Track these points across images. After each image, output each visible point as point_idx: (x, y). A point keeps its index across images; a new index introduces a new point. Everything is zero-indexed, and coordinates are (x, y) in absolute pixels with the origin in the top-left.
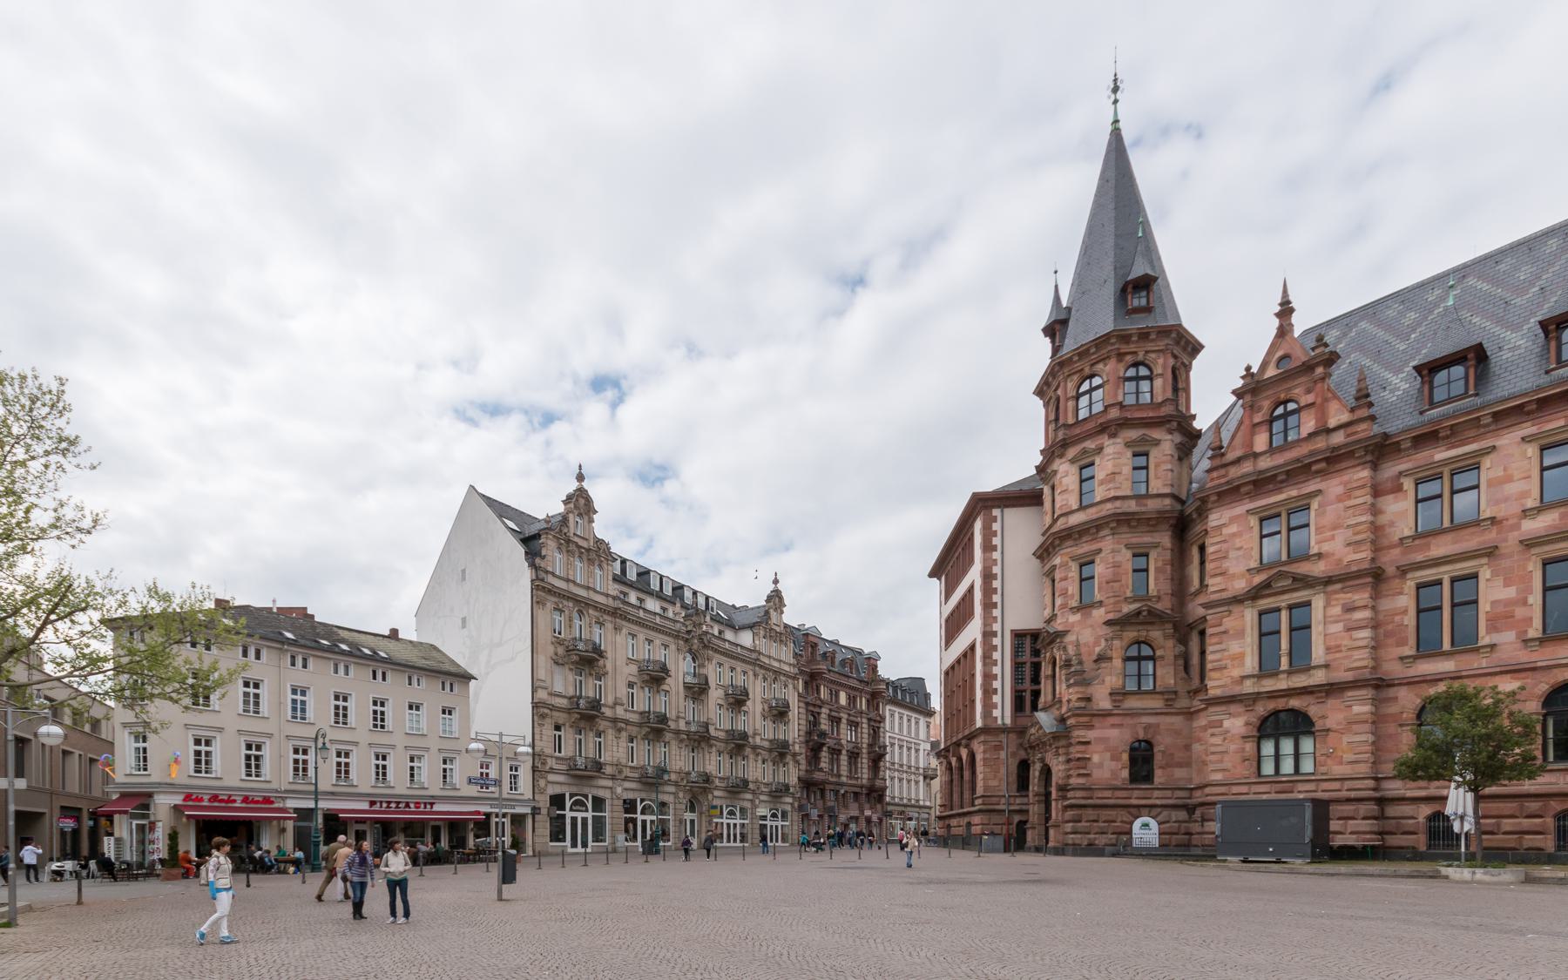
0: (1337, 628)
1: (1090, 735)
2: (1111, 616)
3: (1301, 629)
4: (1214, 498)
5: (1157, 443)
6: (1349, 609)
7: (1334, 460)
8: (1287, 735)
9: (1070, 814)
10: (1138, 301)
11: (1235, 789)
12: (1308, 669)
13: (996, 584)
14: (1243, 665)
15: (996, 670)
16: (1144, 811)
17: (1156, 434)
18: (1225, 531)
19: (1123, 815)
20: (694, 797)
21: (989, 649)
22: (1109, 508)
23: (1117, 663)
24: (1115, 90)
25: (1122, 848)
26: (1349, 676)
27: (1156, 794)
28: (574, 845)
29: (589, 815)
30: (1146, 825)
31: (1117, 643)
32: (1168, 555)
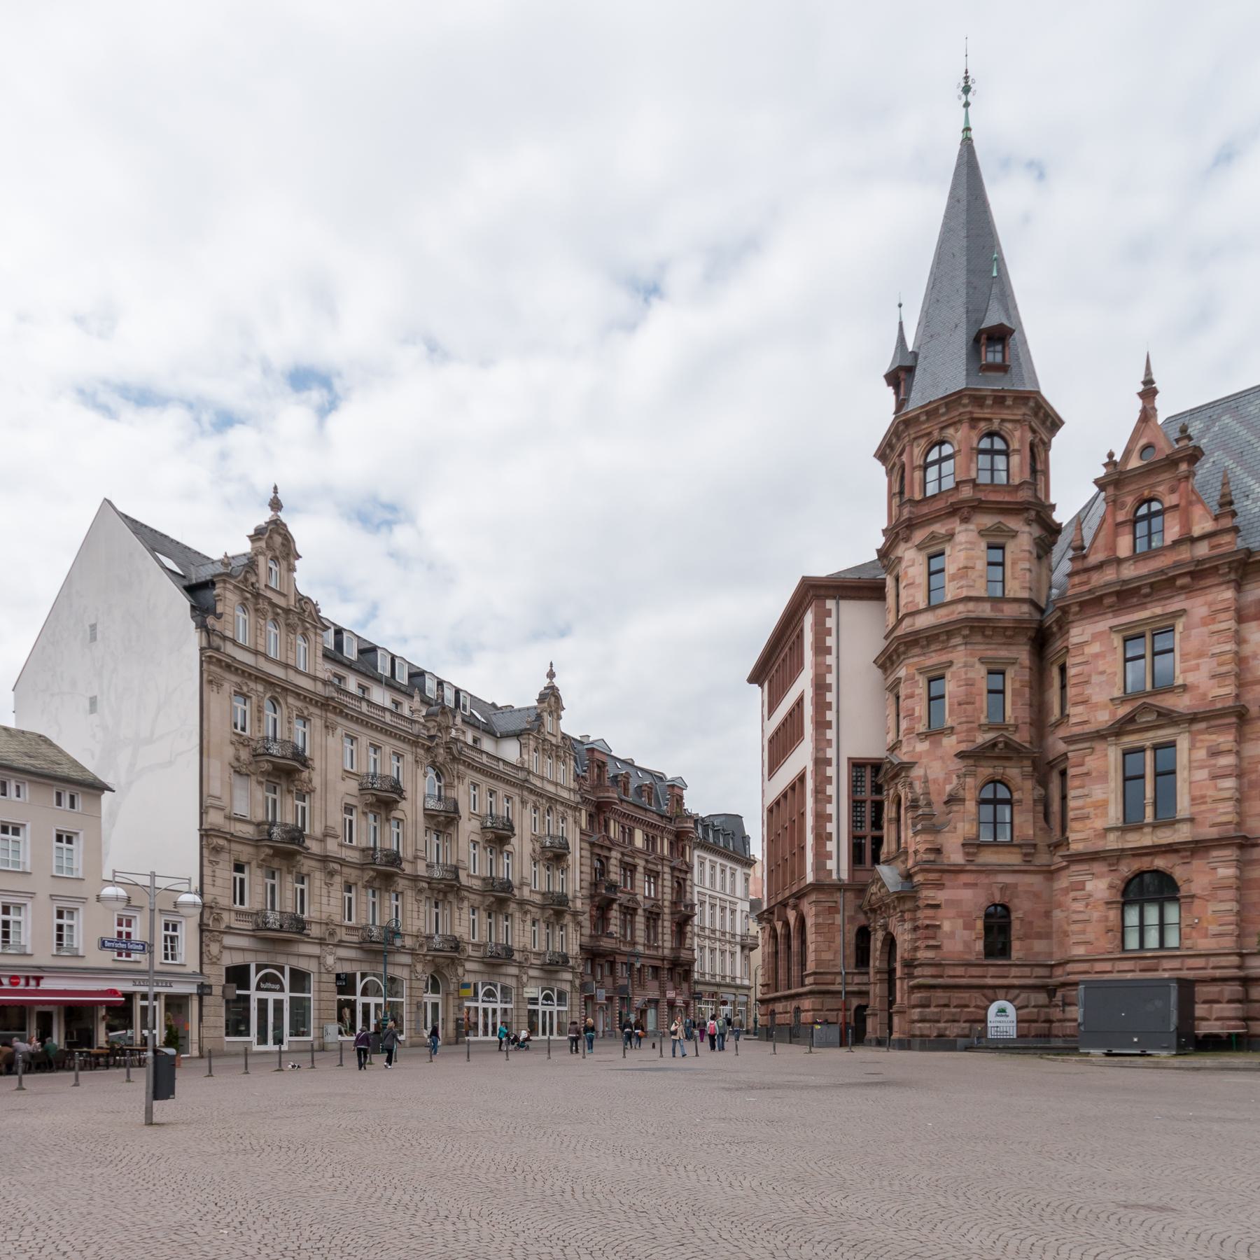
0: (1202, 775)
1: (941, 896)
3: (1166, 774)
4: (1075, 609)
5: (1014, 534)
6: (1215, 753)
7: (1199, 574)
8: (1151, 901)
10: (992, 356)
11: (1099, 966)
12: (1173, 823)
14: (1106, 815)
15: (831, 809)
16: (1001, 992)
17: (1013, 523)
19: (976, 998)
21: (822, 782)
22: (961, 611)
23: (971, 806)
24: (967, 90)
25: (976, 1040)
26: (1212, 833)
28: (263, 1040)
29: (286, 996)
30: (1002, 1011)
31: (969, 780)
32: (1026, 675)
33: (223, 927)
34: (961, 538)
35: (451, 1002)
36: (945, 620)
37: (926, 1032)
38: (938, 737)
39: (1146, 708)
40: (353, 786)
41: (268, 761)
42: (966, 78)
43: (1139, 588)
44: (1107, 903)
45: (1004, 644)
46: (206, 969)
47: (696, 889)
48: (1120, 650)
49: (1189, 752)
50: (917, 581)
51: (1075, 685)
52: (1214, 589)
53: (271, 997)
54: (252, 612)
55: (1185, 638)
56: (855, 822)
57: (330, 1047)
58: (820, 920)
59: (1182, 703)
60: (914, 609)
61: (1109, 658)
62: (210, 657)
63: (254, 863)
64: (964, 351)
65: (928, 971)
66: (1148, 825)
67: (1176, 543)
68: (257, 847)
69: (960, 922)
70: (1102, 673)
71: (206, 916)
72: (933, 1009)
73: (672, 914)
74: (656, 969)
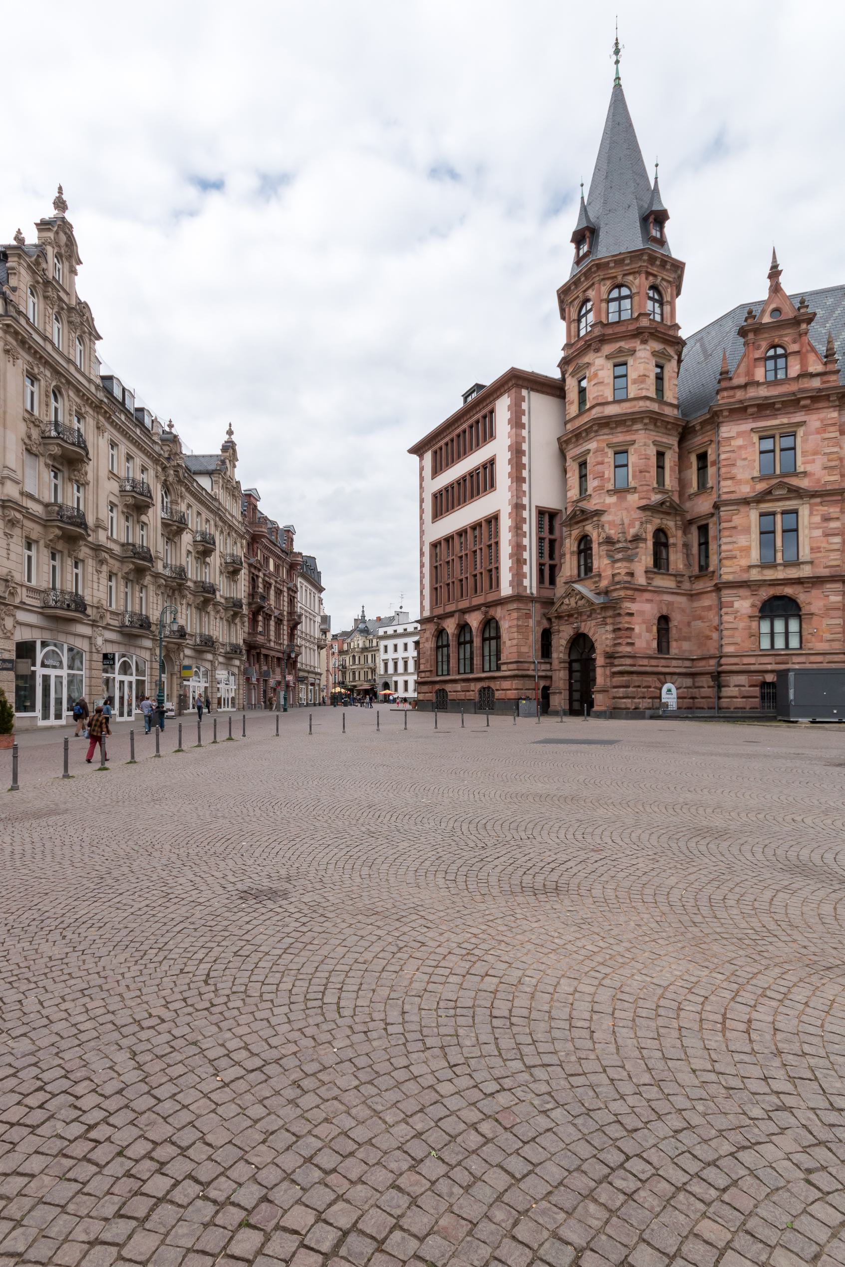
0: (818, 533)
1: (633, 607)
2: (644, 502)
3: (792, 531)
4: (726, 413)
6: (827, 519)
9: (618, 680)
11: (746, 660)
13: (525, 460)
14: (748, 556)
16: (668, 677)
18: (733, 443)
20: (167, 656)
24: (617, 52)
25: (657, 712)
26: (825, 572)
28: (46, 716)
29: (64, 672)
30: (669, 690)
33: (17, 601)
34: (639, 354)
36: (629, 411)
39: (781, 485)
40: (114, 486)
41: (58, 445)
42: (617, 44)
43: (774, 403)
51: (725, 466)
53: (52, 673)
54: (41, 298)
55: (804, 441)
56: (541, 553)
58: (520, 623)
59: (804, 483)
61: (750, 450)
62: (8, 326)
63: (42, 543)
64: (638, 224)
65: (628, 661)
66: (780, 564)
67: (799, 376)
68: (45, 526)
69: (644, 626)
70: (745, 459)
72: (631, 689)
74: (279, 659)
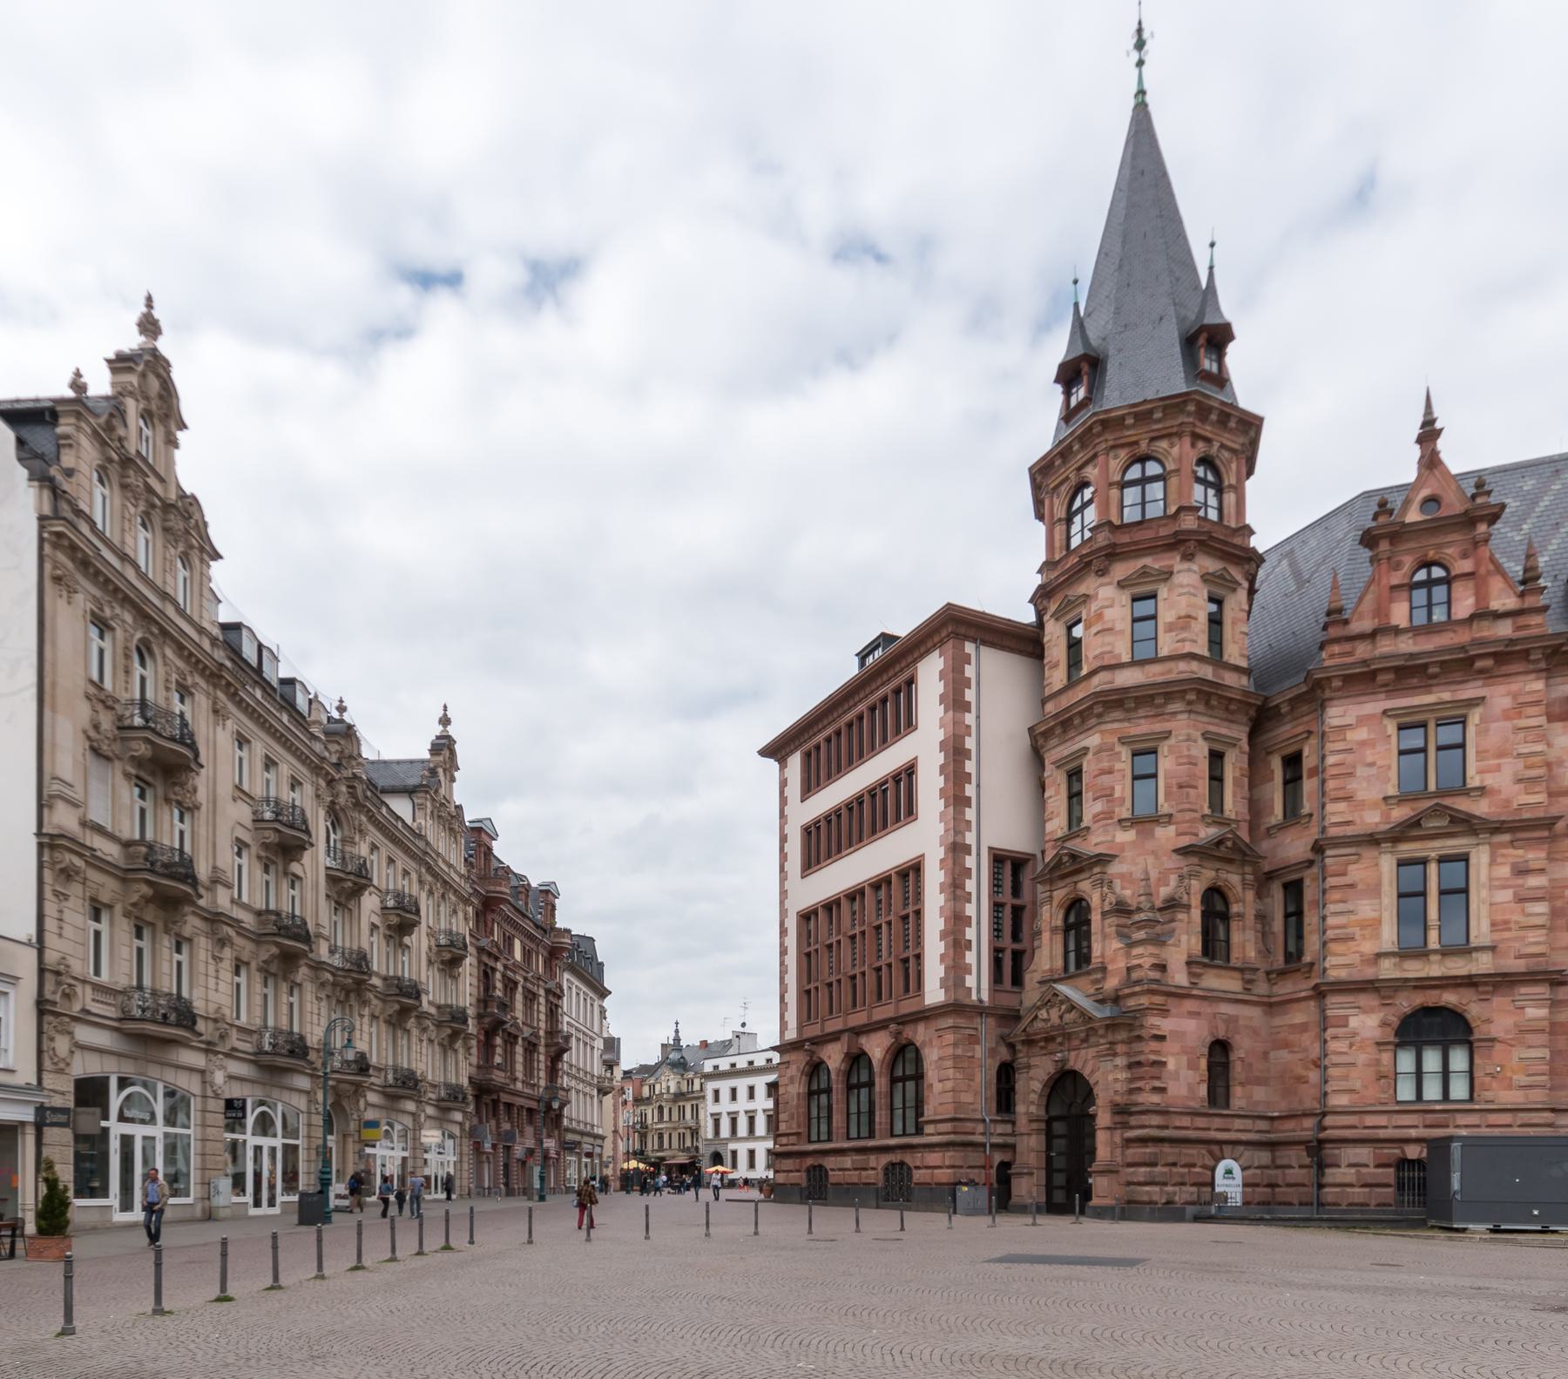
0: (1506, 896)
1: (1165, 1025)
2: (1185, 841)
3: (1458, 893)
4: (1337, 683)
6: (1521, 871)
7: (1507, 657)
8: (1432, 1043)
9: (1135, 1153)
11: (1370, 1120)
14: (1377, 936)
16: (1227, 1149)
18: (1351, 736)
20: (337, 1105)
24: (1140, 45)
25: (1209, 1210)
26: (1519, 966)
27: (1238, 1124)
29: (158, 1130)
30: (1229, 1172)
34: (1179, 579)
35: (351, 1146)
36: (1160, 679)
37: (1155, 1198)
38: (1148, 826)
39: (1438, 810)
40: (244, 812)
42: (1140, 31)
43: (1426, 666)
44: (1378, 1044)
45: (1226, 720)
46: (48, 1080)
47: (566, 1019)
48: (1394, 739)
49: (1487, 866)
50: (1118, 627)
51: (1334, 776)
52: (1521, 678)
53: (138, 1131)
54: (116, 488)
55: (1482, 732)
56: (996, 931)
57: (223, 1213)
58: (959, 1052)
59: (1481, 808)
60: (1113, 662)
61: (1380, 748)
62: (59, 535)
63: (118, 908)
65: (1156, 1120)
66: (1435, 952)
68: (124, 881)
69: (1184, 1059)
70: (1372, 764)
71: (49, 986)
72: (1159, 1169)
73: (547, 1046)
